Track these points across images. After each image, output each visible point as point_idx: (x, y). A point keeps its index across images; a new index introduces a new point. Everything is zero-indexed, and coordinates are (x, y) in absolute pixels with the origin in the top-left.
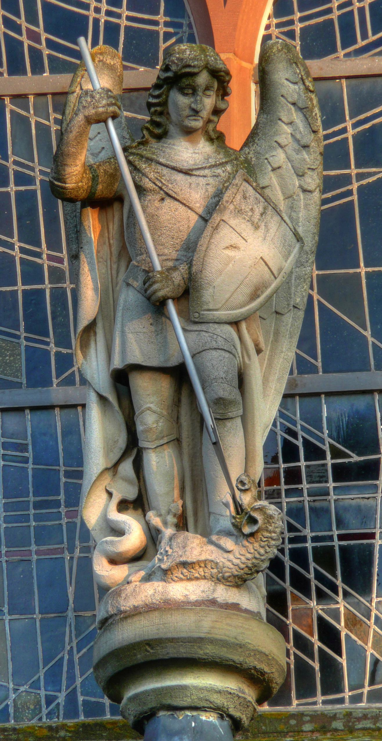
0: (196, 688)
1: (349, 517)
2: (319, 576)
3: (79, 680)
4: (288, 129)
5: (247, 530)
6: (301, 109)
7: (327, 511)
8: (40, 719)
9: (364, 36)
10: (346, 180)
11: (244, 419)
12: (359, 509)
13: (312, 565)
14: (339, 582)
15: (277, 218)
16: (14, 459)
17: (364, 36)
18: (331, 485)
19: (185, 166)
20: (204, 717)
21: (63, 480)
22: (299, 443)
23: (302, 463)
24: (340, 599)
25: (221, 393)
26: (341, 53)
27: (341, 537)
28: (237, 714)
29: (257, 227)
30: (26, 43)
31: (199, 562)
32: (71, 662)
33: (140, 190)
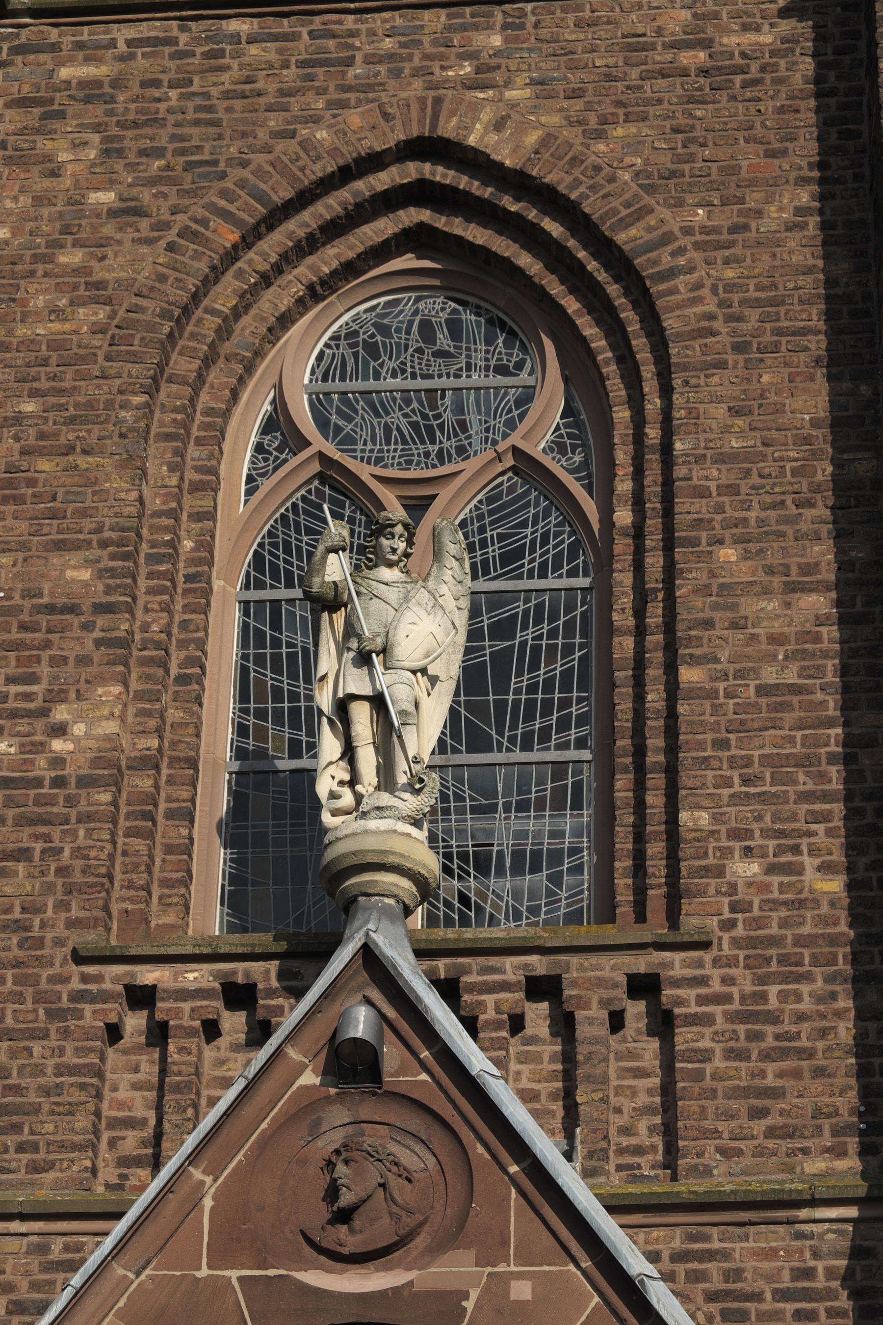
0: (384, 882)
1: (478, 834)
2: (459, 867)
3: (313, 923)
4: (450, 572)
5: (417, 786)
6: (457, 560)
7: (466, 831)
8: (288, 925)
9: (495, 571)
10: (483, 648)
11: (417, 725)
12: (484, 829)
13: (456, 861)
14: (471, 871)
15: (441, 611)
16: (279, 799)
17: (495, 570)
18: (469, 816)
19: (385, 580)
20: (387, 901)
21: (307, 811)
22: (451, 793)
23: (452, 804)
24: (472, 880)
25: (404, 708)
26: (482, 579)
27: (473, 846)
28: (407, 902)
29: (429, 614)
30: (294, 542)
31: (387, 807)
32: (309, 912)
33: (358, 594)
